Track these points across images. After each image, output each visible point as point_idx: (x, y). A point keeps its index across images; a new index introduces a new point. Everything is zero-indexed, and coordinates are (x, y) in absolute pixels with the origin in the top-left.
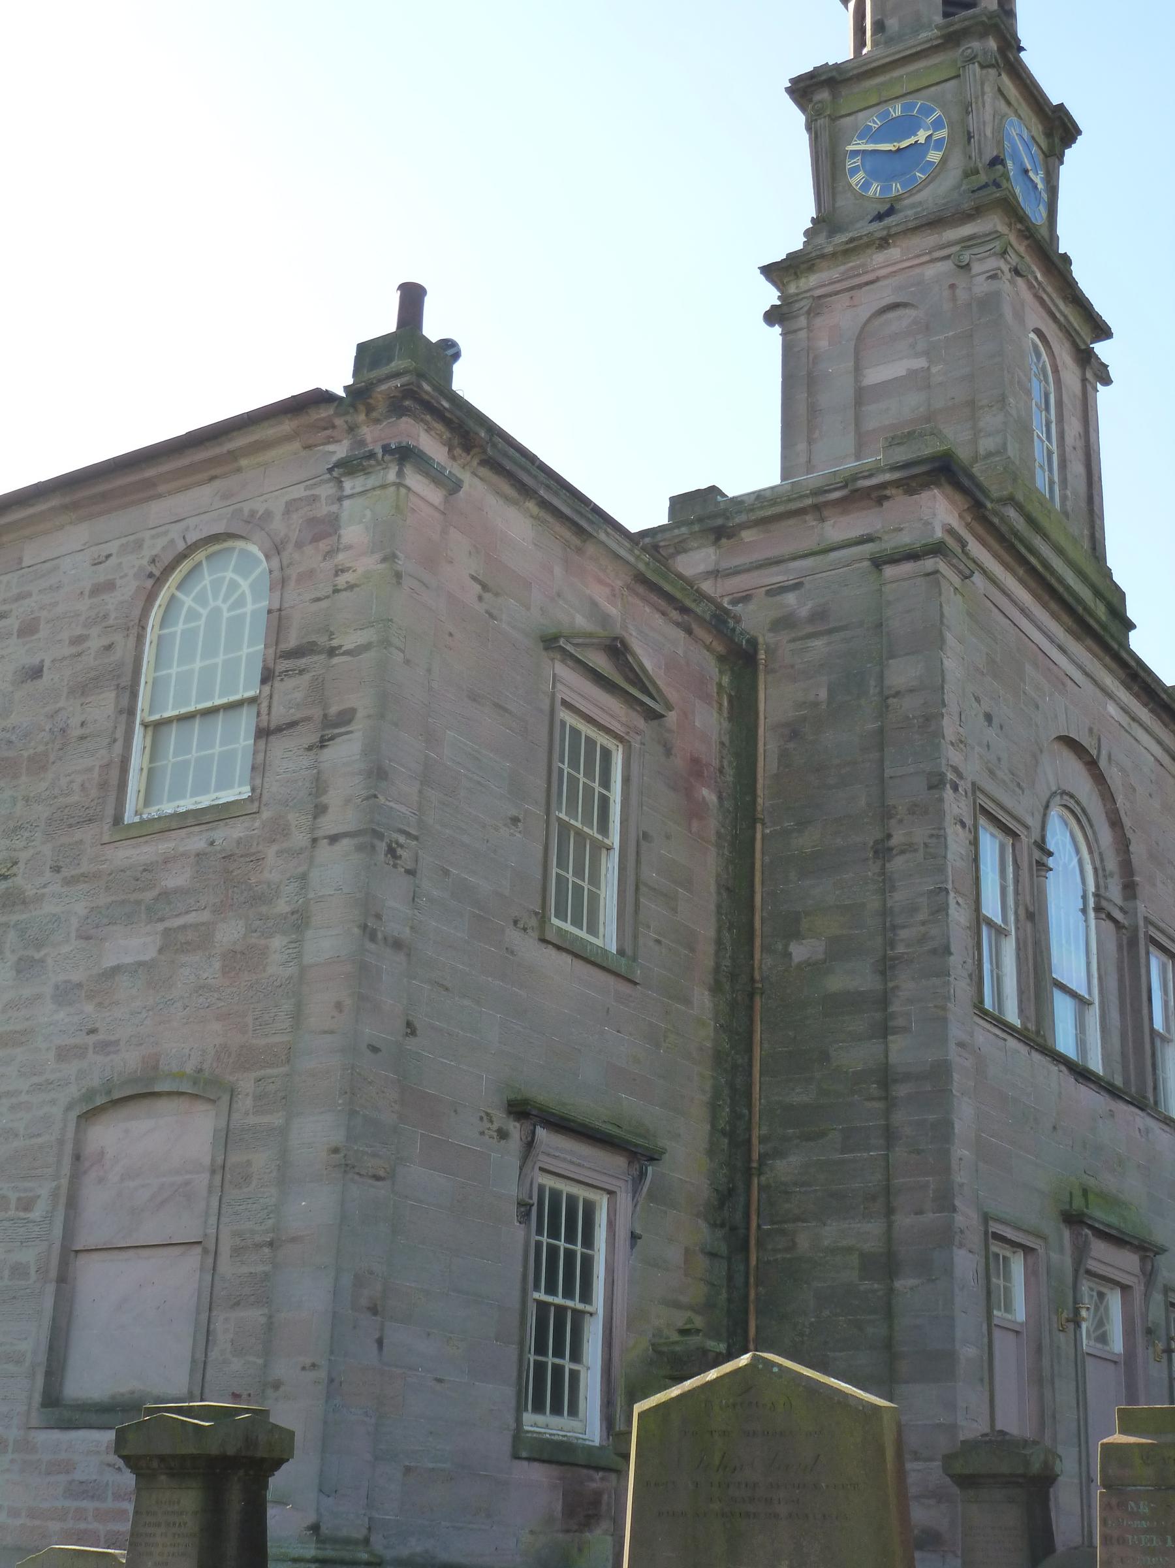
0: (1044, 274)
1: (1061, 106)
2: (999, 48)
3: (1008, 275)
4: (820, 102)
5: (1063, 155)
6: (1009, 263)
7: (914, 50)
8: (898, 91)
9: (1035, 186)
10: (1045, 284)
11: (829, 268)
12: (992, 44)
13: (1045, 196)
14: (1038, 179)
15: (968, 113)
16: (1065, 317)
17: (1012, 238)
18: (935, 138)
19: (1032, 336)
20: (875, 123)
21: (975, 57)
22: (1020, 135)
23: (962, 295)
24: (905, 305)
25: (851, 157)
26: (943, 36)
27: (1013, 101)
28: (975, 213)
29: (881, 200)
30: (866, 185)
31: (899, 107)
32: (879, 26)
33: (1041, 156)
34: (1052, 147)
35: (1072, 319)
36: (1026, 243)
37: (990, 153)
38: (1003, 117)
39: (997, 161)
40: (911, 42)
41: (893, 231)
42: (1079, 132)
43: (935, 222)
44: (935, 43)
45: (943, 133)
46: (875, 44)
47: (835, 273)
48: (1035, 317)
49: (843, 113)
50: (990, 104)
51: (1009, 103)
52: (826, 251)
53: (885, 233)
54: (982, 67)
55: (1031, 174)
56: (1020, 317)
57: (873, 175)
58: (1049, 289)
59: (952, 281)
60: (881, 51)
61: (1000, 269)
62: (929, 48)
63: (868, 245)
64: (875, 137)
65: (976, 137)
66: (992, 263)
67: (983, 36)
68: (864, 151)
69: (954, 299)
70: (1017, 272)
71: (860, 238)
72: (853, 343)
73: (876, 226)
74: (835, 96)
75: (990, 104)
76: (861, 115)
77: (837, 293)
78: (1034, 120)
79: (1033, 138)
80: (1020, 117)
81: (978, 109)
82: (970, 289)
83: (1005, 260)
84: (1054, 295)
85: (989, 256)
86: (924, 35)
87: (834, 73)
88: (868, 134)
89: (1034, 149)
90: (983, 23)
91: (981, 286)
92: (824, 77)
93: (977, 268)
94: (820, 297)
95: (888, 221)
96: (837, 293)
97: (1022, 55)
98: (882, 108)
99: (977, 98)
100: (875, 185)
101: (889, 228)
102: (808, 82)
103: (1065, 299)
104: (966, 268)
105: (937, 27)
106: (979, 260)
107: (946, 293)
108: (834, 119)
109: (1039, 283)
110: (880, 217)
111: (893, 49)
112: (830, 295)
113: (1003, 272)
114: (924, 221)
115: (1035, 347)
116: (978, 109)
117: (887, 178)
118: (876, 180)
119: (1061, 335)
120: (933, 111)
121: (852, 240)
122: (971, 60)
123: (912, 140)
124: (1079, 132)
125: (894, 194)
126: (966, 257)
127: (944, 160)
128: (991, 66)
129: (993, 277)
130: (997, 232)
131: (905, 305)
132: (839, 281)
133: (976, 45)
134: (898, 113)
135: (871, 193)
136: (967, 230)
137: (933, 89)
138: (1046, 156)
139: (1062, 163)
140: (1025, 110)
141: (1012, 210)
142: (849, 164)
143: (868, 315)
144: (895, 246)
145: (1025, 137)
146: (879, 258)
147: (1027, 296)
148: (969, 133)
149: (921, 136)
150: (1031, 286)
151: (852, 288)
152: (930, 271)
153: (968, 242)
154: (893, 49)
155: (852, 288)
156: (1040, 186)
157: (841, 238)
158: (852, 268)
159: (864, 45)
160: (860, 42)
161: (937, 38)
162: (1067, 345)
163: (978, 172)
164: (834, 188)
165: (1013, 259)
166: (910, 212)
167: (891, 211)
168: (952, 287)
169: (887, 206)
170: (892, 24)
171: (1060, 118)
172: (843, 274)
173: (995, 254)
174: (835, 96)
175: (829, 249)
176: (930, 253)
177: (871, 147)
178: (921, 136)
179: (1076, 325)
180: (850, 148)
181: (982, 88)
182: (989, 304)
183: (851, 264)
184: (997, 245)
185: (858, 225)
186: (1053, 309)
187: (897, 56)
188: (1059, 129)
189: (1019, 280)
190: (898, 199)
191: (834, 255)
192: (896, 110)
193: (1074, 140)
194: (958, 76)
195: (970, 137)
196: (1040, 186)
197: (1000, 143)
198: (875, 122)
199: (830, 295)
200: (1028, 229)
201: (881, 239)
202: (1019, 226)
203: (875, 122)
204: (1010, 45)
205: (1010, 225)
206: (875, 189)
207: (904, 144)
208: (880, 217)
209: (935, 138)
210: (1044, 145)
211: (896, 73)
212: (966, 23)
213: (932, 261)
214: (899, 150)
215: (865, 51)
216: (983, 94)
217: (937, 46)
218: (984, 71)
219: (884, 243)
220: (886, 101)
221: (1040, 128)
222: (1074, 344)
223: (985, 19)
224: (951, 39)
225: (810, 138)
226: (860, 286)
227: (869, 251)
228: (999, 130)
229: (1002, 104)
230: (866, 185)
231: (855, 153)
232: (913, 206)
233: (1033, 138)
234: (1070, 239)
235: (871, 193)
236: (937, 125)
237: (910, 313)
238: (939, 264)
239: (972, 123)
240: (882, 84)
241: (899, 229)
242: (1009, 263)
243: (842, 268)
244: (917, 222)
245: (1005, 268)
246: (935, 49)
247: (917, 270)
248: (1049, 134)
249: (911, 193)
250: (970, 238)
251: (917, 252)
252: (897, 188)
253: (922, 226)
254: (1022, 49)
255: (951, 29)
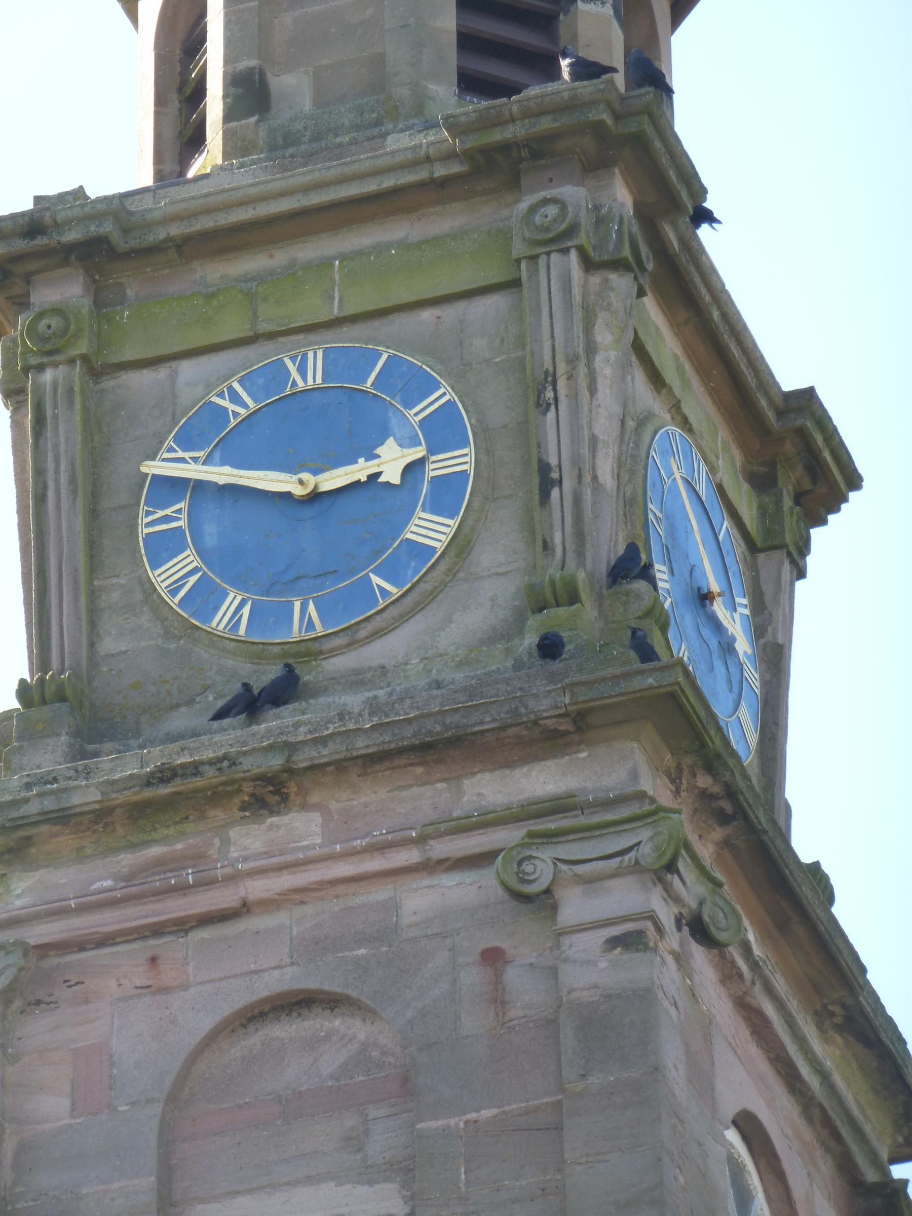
0: (764, 934)
1: (807, 399)
2: (637, 205)
3: (674, 939)
4: (57, 311)
5: (804, 547)
6: (677, 900)
7: (371, 186)
8: (311, 306)
9: (728, 647)
10: (188, 786)
11: (80, 857)
12: (621, 195)
13: (753, 675)
14: (735, 620)
15: (543, 407)
16: (825, 1077)
17: (685, 824)
18: (433, 470)
19: (732, 1136)
20: (239, 402)
21: (572, 231)
22: (688, 481)
23: (524, 988)
24: (332, 1002)
25: (156, 502)
26: (468, 155)
27: (670, 375)
28: (571, 731)
29: (256, 652)
30: (205, 597)
31: (316, 361)
32: (250, 93)
33: (740, 547)
34: (770, 517)
35: (838, 1079)
36: (718, 833)
37: (608, 545)
38: (642, 422)
39: (631, 567)
40: (363, 161)
41: (302, 759)
42: (854, 481)
43: (440, 746)
44: (440, 171)
45: (461, 460)
46: (235, 146)
47: (101, 875)
48: (743, 1082)
49: (130, 354)
50: (610, 391)
51: (656, 379)
52: (76, 800)
53: (276, 762)
54: (589, 265)
55: (719, 608)
56: (702, 1079)
57: (229, 565)
58: (780, 984)
59: (491, 940)
60: (249, 177)
61: (652, 917)
62: (422, 185)
63: (215, 797)
64: (234, 446)
65: (567, 484)
66: (627, 897)
67: (595, 167)
68: (199, 486)
69: (498, 998)
70: (698, 929)
71: (195, 769)
72: (157, 1109)
73: (231, 736)
74: (103, 300)
75: (610, 391)
76: (188, 369)
77: (105, 941)
78: (723, 434)
79: (721, 489)
80: (685, 424)
81: (574, 396)
82: (554, 972)
83: (668, 889)
84: (793, 1005)
85: (616, 874)
86: (400, 142)
87: (108, 228)
88: (204, 430)
89: (725, 526)
90: (598, 129)
91: (591, 969)
92: (72, 236)
93: (574, 906)
94: (44, 949)
95: (277, 722)
96: (105, 941)
97: (704, 232)
98: (257, 357)
99: (572, 361)
100: (233, 599)
101: (291, 748)
102: (20, 245)
103: (821, 1017)
104: (538, 902)
105: (454, 126)
106: (581, 880)
107: (473, 977)
108: (97, 370)
109: (754, 965)
110: (250, 704)
111: (301, 176)
112: (81, 945)
113: (659, 929)
114: (408, 737)
115: (737, 1170)
116: (574, 396)
117: (276, 585)
118: (239, 583)
119: (807, 1133)
120: (431, 386)
121: (166, 774)
122: (559, 239)
123: (359, 471)
124: (854, 481)
125: (296, 632)
126: (542, 868)
127: (461, 545)
128: (617, 265)
129: (631, 942)
130: (641, 796)
131: (332, 1002)
132: (112, 903)
133: (574, 193)
134: (315, 377)
135: (220, 622)
136: (542, 780)
137: (427, 315)
138: (752, 547)
139: (801, 574)
140: (699, 404)
141: (681, 723)
142: (148, 523)
143: (206, 1023)
144: (304, 807)
145: (703, 489)
146: (250, 839)
147: (718, 1003)
148: (544, 468)
149: (391, 461)
150: (729, 974)
151: (157, 931)
152: (420, 900)
153: (548, 819)
154: (301, 176)
155: (157, 931)
156: (743, 646)
157: (122, 766)
158: (160, 864)
159: (195, 140)
160: (180, 134)
161: (450, 156)
162: (826, 1167)
163: (573, 598)
164: (93, 594)
165: (690, 887)
166: (354, 701)
167: (285, 690)
168: (493, 957)
169: (272, 672)
170: (293, 87)
171: (802, 434)
172: (129, 878)
173: (637, 868)
174: (103, 300)
175: (86, 796)
176: (422, 840)
177: (222, 474)
178: (391, 461)
179: (850, 1099)
180: (153, 468)
181: (588, 330)
182: (614, 1029)
183: (155, 851)
184: (645, 841)
185: (178, 721)
186: (792, 1049)
187: (316, 199)
188: (794, 465)
189: (699, 955)
190: (311, 650)
191: (101, 816)
192: (308, 369)
193: (835, 501)
194: (515, 284)
195: (547, 481)
196: (743, 646)
197: (633, 505)
198: (235, 398)
199: (81, 945)
200: (731, 793)
201: (264, 779)
202: (704, 781)
203: (235, 398)
204: (674, 198)
205: (675, 778)
206: (232, 612)
207: (333, 480)
208: (250, 704)
209: (433, 470)
210: (748, 514)
211: (308, 251)
212: (546, 124)
213: (429, 867)
214: (316, 496)
215: (198, 166)
216: (591, 349)
217: (444, 183)
218: (595, 280)
219: (270, 793)
220: (272, 336)
221: (738, 457)
222: (846, 1167)
223: (607, 118)
224: (495, 168)
225: (16, 425)
226: (183, 926)
227: (218, 815)
228: (633, 465)
229: (643, 394)
230: (205, 597)
231: (172, 487)
232: (356, 680)
233: (721, 489)
234: (827, 816)
235: (220, 622)
236: (440, 432)
237: (359, 1030)
238: (449, 880)
239: (556, 441)
240: (261, 278)
241: (324, 754)
242: (677, 900)
243: (126, 860)
244: (385, 740)
245: (666, 914)
246: (437, 191)
247: (381, 893)
248: (762, 481)
249: (353, 638)
250: (559, 806)
251: (379, 834)
252: (305, 618)
253: (401, 751)
254: (707, 217)
255: (497, 136)
